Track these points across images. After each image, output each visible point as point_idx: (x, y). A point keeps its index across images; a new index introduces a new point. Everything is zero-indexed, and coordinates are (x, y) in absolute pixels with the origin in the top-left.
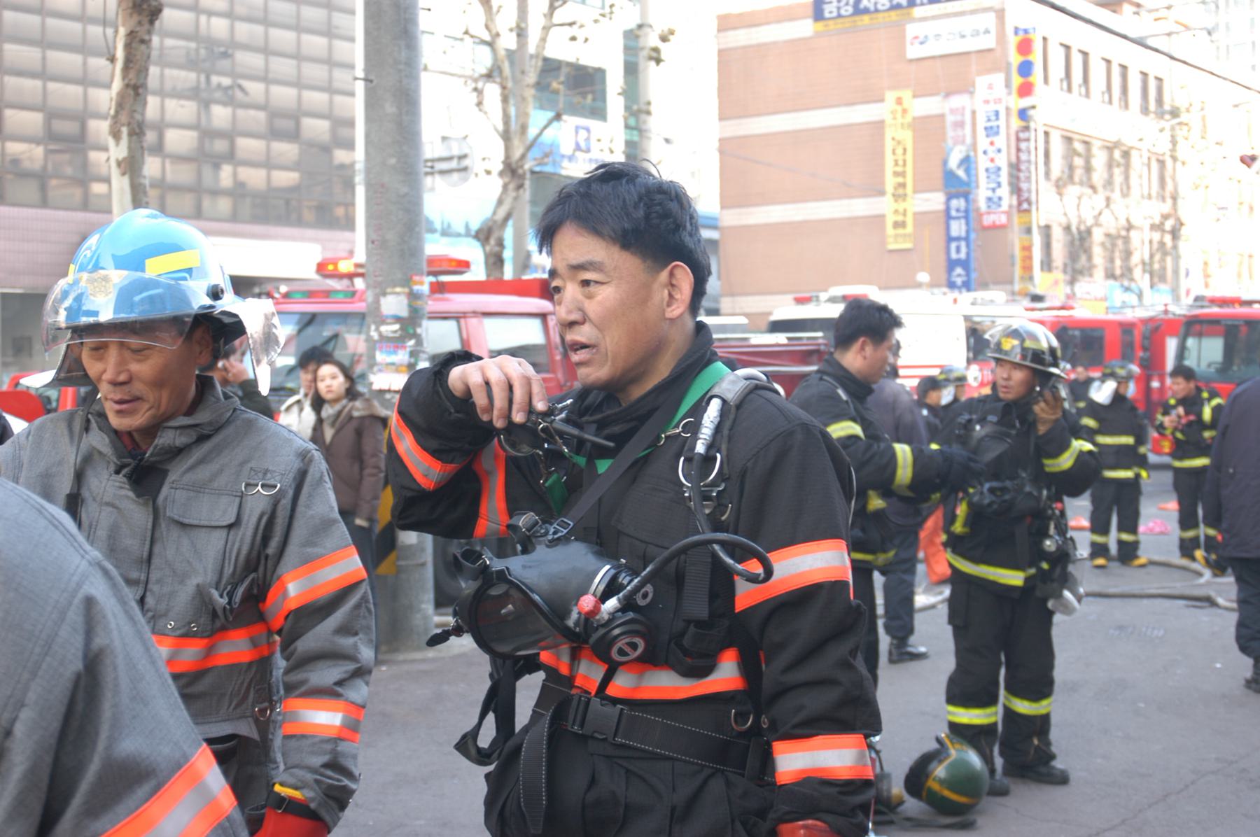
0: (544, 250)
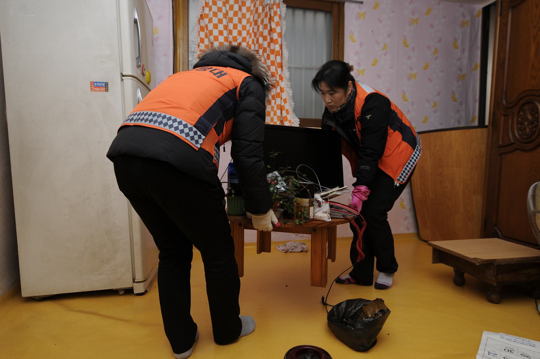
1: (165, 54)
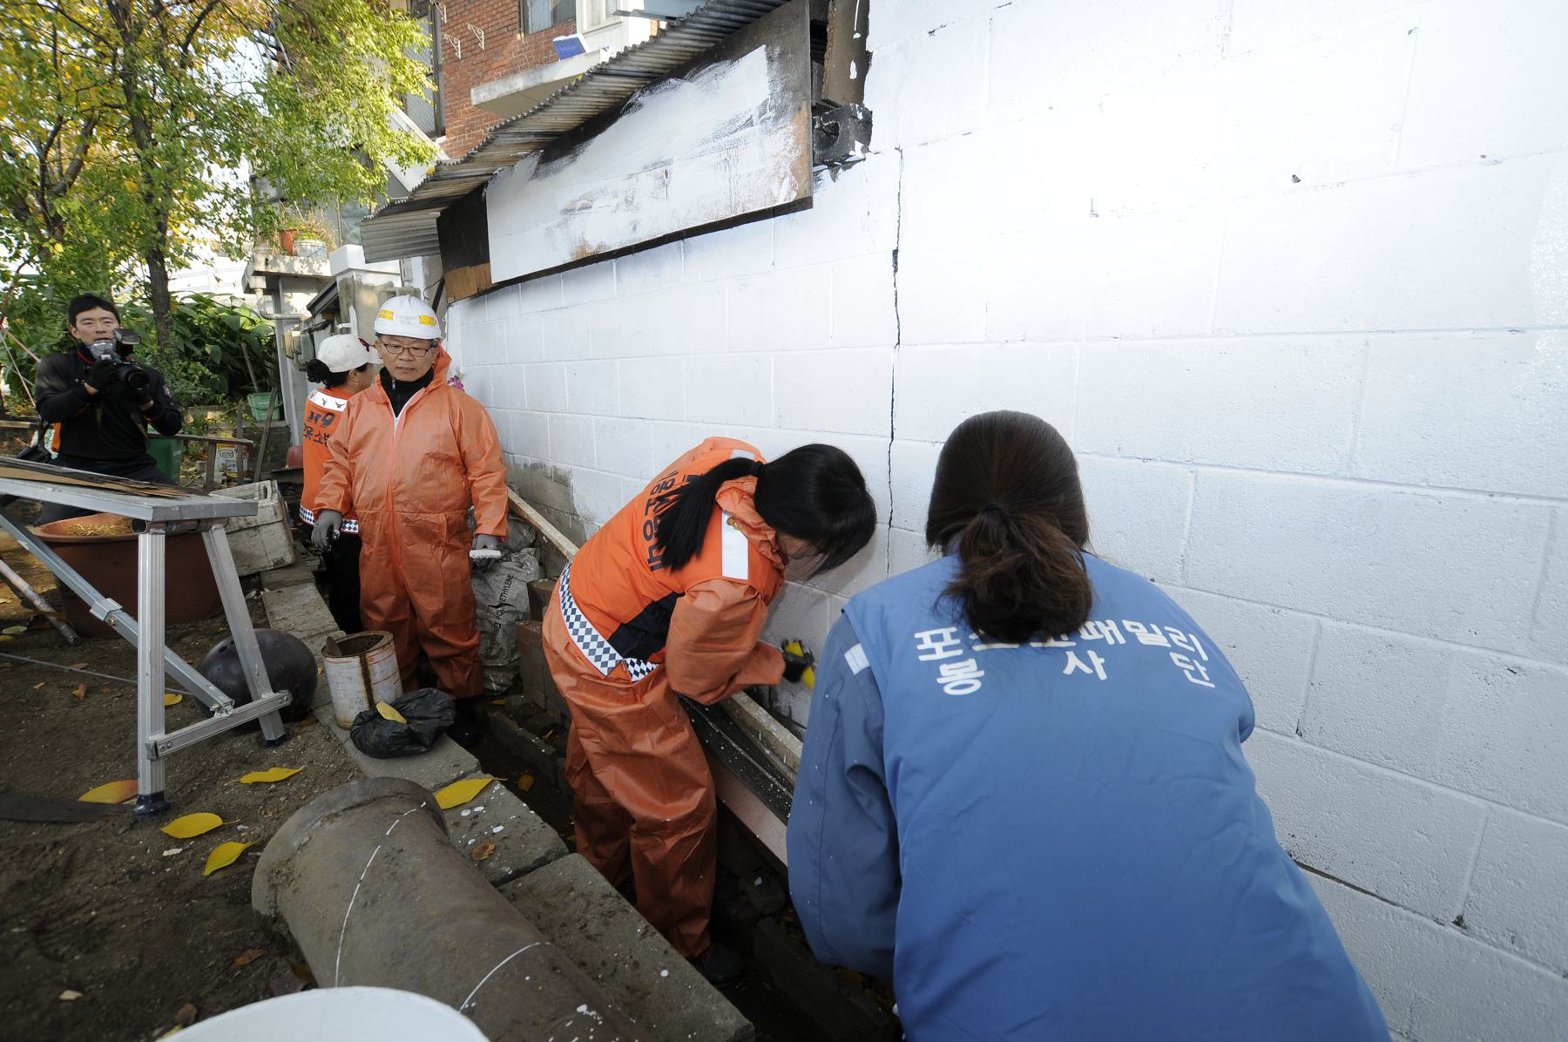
0: (477, 531)
1: (458, 823)
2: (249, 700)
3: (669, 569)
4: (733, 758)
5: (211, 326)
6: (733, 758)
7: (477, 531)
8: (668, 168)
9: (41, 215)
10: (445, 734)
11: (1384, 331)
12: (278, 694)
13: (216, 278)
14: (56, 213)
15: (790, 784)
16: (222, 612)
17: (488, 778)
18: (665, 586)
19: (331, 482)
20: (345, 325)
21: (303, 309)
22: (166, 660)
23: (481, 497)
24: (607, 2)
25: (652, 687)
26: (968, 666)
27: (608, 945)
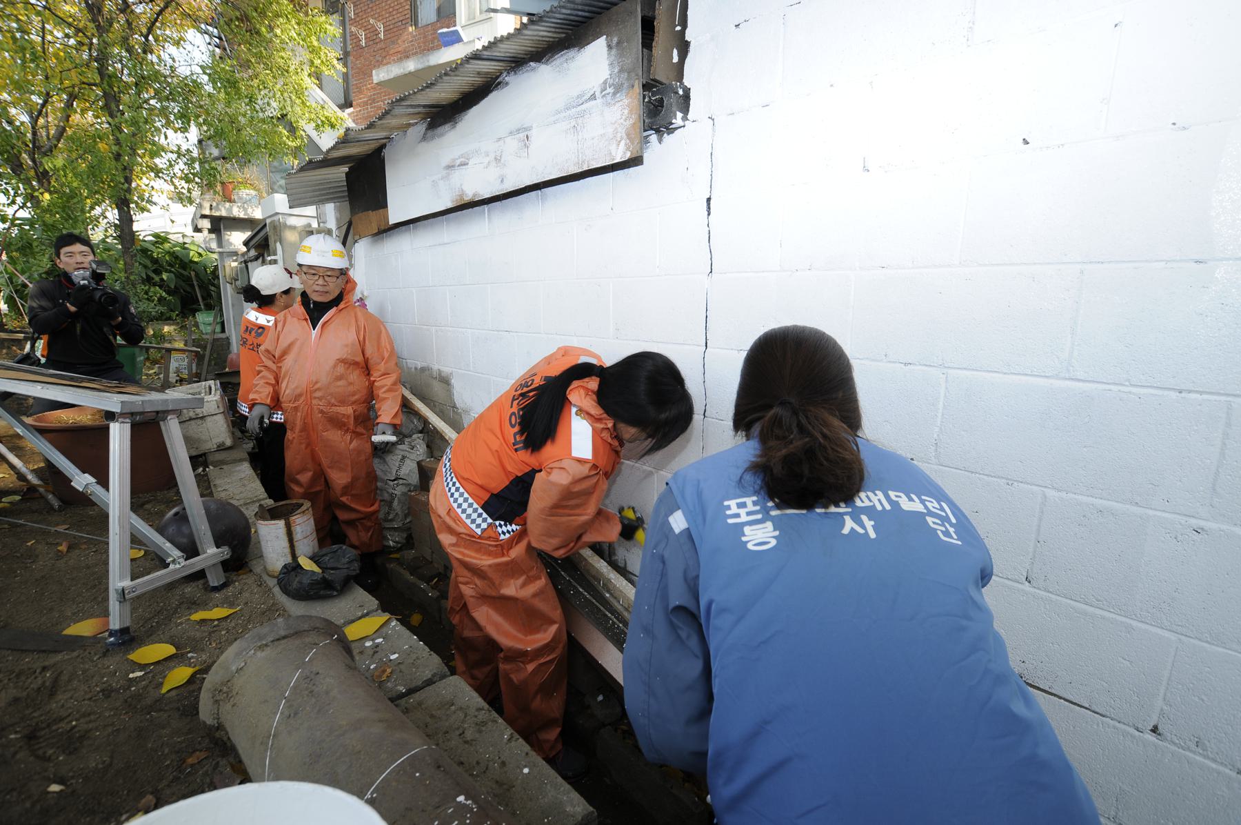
0: (378, 421)
1: (362, 651)
2: (197, 554)
3: (530, 451)
4: (580, 600)
5: (167, 258)
6: (580, 600)
7: (378, 421)
8: (529, 133)
9: (33, 170)
10: (352, 581)
11: (1096, 262)
12: (220, 549)
13: (171, 220)
14: (45, 169)
15: (625, 620)
16: (176, 485)
17: (386, 616)
18: (526, 464)
19: (262, 382)
20: (273, 257)
21: (240, 245)
22: (131, 523)
23: (381, 393)
24: (480, 1)
25: (516, 544)
26: (766, 528)
27: (481, 748)
